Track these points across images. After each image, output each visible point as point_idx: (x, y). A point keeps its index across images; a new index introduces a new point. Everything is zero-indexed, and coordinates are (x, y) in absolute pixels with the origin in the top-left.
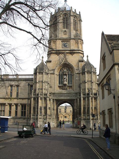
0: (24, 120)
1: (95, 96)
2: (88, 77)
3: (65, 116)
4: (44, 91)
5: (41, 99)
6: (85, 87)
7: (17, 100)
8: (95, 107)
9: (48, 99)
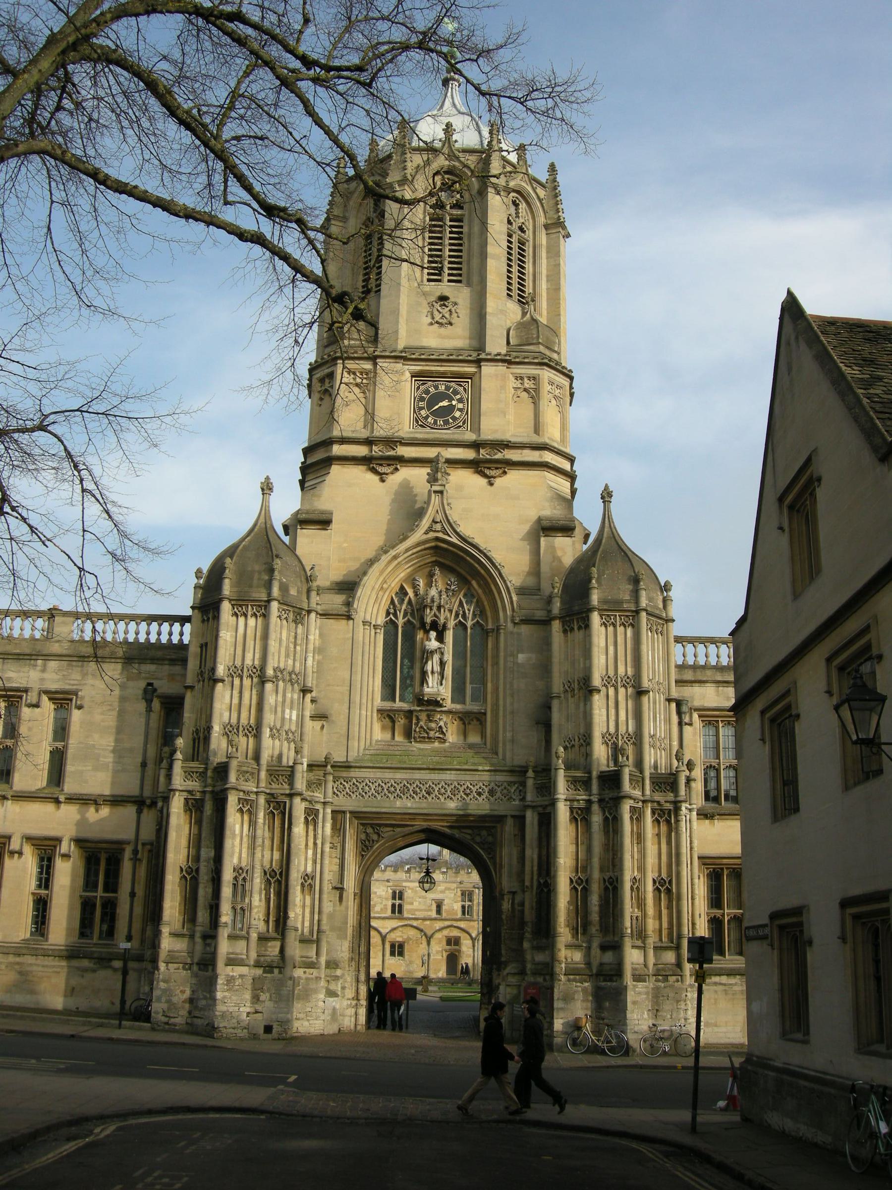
0: (102, 973)
1: (658, 797)
2: (611, 649)
3: (393, 946)
4: (270, 746)
5: (248, 807)
6: (589, 725)
7: (50, 807)
8: (662, 882)
9: (299, 808)
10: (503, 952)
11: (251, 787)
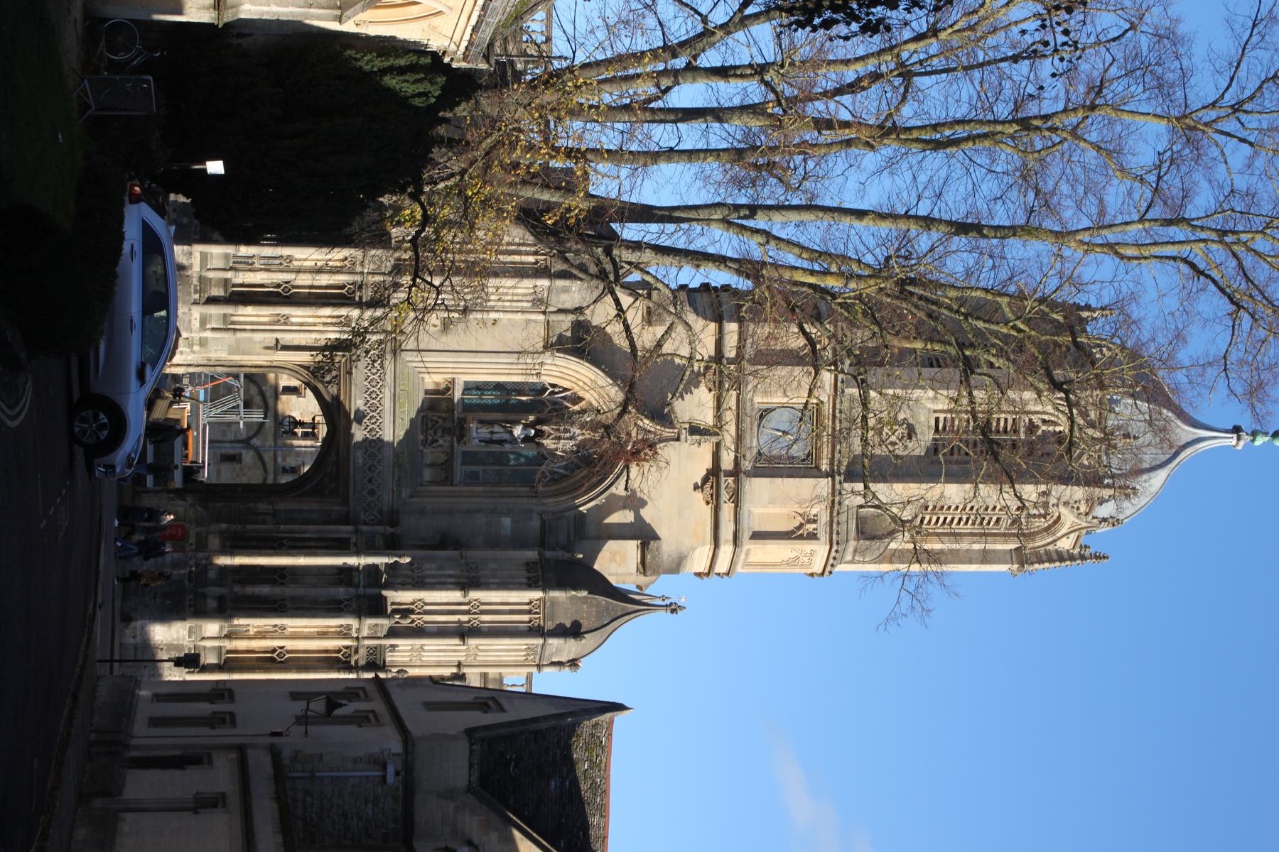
1: (362, 651)
10: (219, 505)
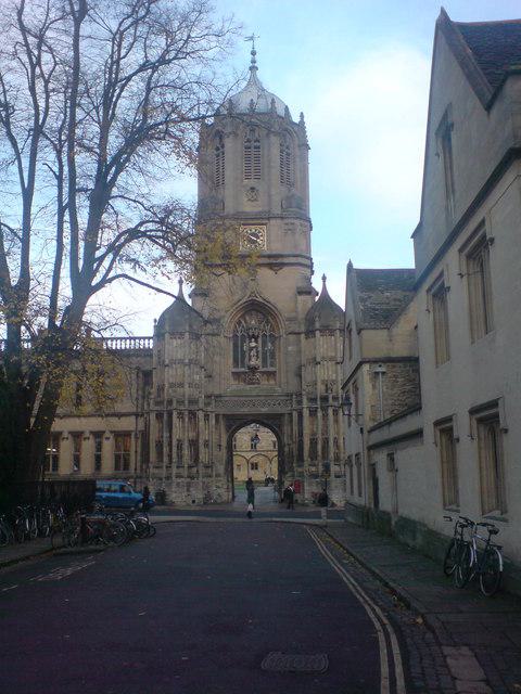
9: (201, 415)
11: (182, 408)
